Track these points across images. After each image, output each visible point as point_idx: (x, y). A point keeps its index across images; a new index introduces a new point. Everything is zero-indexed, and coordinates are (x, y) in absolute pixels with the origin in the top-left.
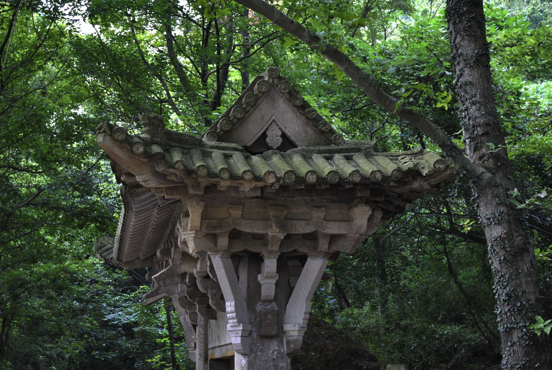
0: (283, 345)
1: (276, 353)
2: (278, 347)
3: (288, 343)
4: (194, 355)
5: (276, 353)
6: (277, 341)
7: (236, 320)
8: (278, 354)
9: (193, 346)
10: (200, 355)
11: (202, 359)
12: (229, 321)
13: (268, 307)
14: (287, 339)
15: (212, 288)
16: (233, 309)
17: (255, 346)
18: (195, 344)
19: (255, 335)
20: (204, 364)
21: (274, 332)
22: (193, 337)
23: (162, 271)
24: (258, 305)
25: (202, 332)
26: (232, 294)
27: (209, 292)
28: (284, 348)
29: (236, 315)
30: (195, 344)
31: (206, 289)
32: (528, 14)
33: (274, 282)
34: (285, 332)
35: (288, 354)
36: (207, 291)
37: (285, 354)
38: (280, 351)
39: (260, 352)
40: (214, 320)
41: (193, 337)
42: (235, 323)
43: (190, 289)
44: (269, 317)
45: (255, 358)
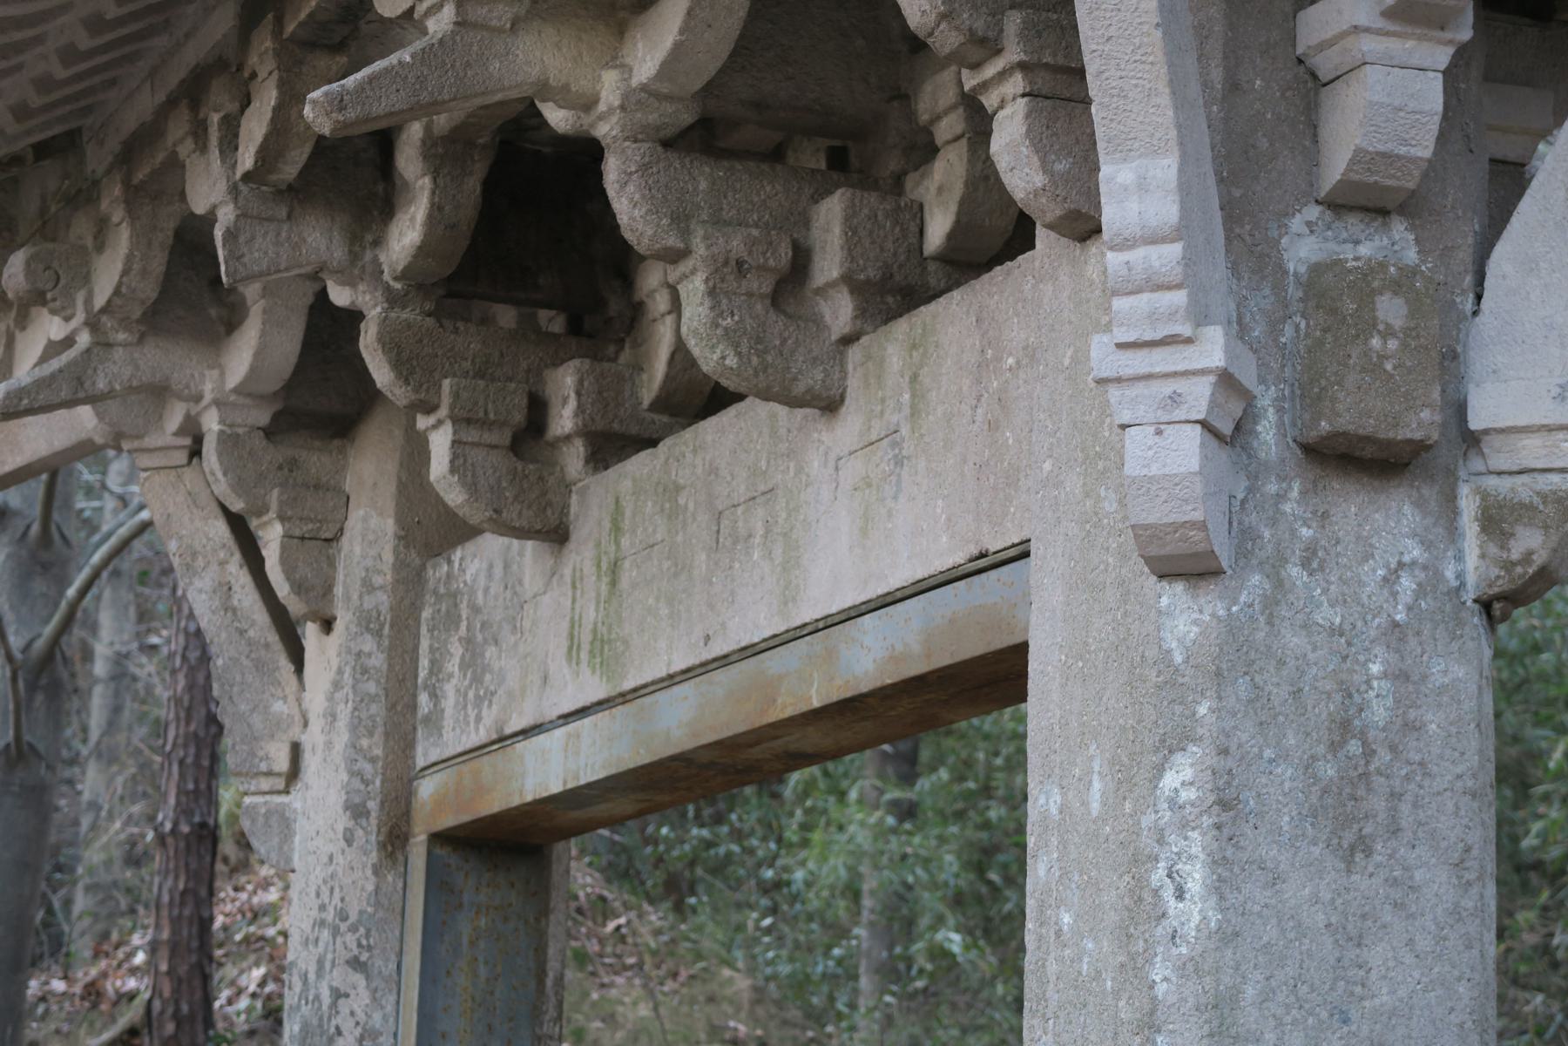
0: (1453, 532)
1: (1407, 583)
2: (1427, 545)
3: (1496, 521)
4: (284, 823)
5: (1407, 583)
6: (1419, 504)
7: (1180, 298)
8: (1421, 591)
9: (282, 763)
10: (357, 811)
11: (369, 836)
12: (1119, 304)
13: (1364, 250)
14: (1484, 495)
15: (717, 221)
16: (1166, 211)
17: (1273, 523)
18: (296, 750)
19: (1268, 434)
20: (376, 871)
21: (1422, 422)
22: (278, 707)
23: (379, 65)
24: (1297, 223)
25: (378, 661)
26: (1165, 99)
27: (700, 249)
28: (1460, 558)
29: (1188, 261)
30: (296, 750)
31: (681, 221)
32: (617, 103)
33: (1442, 57)
34: (1472, 441)
35: (1486, 605)
36: (685, 233)
37: (1469, 596)
38: (1438, 576)
39: (1305, 564)
40: (529, 552)
41: (278, 707)
42: (1172, 315)
43: (406, 315)
44: (1391, 309)
45: (1270, 604)
